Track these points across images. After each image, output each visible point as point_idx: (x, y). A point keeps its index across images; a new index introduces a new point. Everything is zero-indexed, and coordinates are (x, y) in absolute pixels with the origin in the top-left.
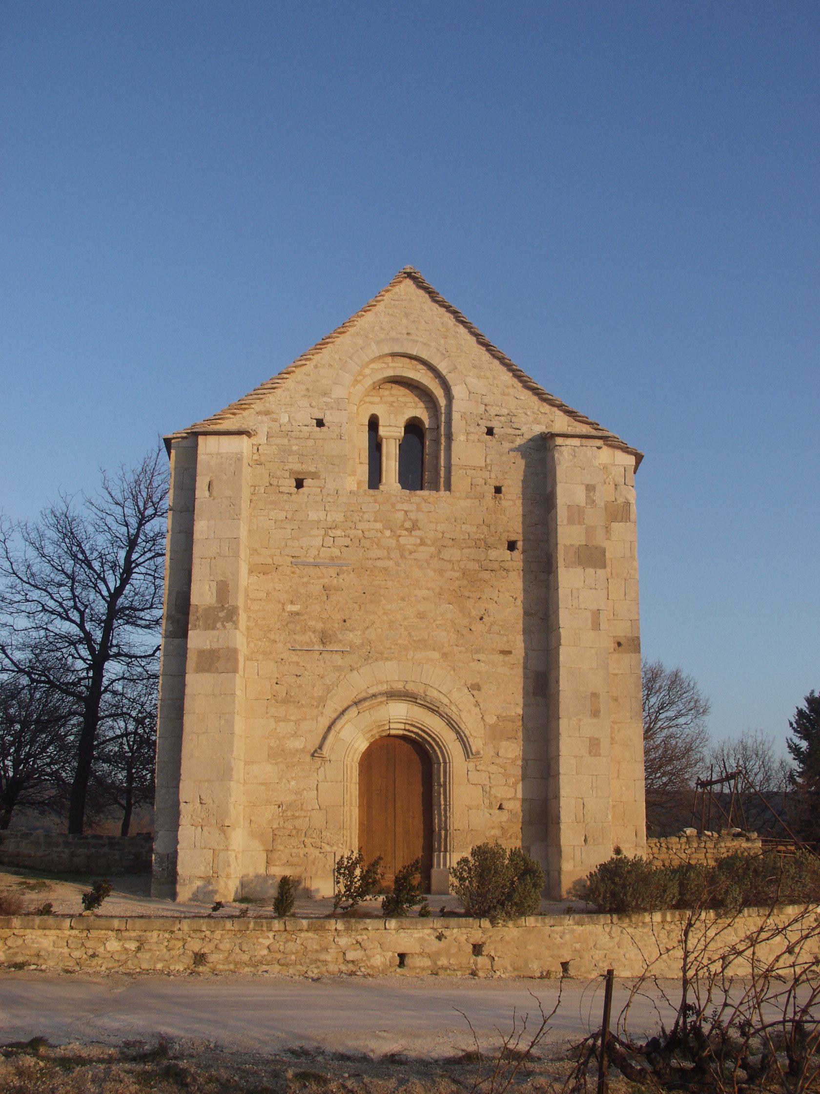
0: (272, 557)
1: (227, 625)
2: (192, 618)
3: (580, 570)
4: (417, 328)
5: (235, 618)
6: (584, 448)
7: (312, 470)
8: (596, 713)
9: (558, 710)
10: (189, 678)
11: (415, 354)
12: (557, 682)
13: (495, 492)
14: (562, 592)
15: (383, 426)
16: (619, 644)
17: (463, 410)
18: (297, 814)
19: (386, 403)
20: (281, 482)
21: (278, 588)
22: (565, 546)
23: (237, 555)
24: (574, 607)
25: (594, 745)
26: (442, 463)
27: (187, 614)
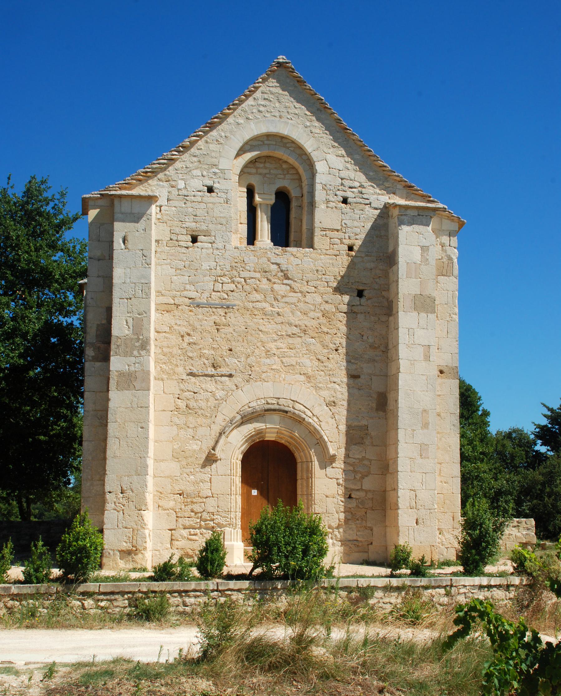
0: (174, 298)
1: (142, 352)
2: (113, 346)
3: (415, 314)
5: (148, 347)
6: (421, 217)
8: (425, 426)
9: (397, 423)
10: (111, 394)
11: (286, 134)
12: (397, 401)
13: (349, 250)
14: (402, 332)
16: (441, 372)
17: (324, 183)
18: (195, 500)
19: (260, 174)
20: (180, 237)
21: (179, 324)
22: (404, 295)
23: (148, 296)
24: (410, 343)
25: (423, 449)
26: (304, 227)
27: (109, 343)
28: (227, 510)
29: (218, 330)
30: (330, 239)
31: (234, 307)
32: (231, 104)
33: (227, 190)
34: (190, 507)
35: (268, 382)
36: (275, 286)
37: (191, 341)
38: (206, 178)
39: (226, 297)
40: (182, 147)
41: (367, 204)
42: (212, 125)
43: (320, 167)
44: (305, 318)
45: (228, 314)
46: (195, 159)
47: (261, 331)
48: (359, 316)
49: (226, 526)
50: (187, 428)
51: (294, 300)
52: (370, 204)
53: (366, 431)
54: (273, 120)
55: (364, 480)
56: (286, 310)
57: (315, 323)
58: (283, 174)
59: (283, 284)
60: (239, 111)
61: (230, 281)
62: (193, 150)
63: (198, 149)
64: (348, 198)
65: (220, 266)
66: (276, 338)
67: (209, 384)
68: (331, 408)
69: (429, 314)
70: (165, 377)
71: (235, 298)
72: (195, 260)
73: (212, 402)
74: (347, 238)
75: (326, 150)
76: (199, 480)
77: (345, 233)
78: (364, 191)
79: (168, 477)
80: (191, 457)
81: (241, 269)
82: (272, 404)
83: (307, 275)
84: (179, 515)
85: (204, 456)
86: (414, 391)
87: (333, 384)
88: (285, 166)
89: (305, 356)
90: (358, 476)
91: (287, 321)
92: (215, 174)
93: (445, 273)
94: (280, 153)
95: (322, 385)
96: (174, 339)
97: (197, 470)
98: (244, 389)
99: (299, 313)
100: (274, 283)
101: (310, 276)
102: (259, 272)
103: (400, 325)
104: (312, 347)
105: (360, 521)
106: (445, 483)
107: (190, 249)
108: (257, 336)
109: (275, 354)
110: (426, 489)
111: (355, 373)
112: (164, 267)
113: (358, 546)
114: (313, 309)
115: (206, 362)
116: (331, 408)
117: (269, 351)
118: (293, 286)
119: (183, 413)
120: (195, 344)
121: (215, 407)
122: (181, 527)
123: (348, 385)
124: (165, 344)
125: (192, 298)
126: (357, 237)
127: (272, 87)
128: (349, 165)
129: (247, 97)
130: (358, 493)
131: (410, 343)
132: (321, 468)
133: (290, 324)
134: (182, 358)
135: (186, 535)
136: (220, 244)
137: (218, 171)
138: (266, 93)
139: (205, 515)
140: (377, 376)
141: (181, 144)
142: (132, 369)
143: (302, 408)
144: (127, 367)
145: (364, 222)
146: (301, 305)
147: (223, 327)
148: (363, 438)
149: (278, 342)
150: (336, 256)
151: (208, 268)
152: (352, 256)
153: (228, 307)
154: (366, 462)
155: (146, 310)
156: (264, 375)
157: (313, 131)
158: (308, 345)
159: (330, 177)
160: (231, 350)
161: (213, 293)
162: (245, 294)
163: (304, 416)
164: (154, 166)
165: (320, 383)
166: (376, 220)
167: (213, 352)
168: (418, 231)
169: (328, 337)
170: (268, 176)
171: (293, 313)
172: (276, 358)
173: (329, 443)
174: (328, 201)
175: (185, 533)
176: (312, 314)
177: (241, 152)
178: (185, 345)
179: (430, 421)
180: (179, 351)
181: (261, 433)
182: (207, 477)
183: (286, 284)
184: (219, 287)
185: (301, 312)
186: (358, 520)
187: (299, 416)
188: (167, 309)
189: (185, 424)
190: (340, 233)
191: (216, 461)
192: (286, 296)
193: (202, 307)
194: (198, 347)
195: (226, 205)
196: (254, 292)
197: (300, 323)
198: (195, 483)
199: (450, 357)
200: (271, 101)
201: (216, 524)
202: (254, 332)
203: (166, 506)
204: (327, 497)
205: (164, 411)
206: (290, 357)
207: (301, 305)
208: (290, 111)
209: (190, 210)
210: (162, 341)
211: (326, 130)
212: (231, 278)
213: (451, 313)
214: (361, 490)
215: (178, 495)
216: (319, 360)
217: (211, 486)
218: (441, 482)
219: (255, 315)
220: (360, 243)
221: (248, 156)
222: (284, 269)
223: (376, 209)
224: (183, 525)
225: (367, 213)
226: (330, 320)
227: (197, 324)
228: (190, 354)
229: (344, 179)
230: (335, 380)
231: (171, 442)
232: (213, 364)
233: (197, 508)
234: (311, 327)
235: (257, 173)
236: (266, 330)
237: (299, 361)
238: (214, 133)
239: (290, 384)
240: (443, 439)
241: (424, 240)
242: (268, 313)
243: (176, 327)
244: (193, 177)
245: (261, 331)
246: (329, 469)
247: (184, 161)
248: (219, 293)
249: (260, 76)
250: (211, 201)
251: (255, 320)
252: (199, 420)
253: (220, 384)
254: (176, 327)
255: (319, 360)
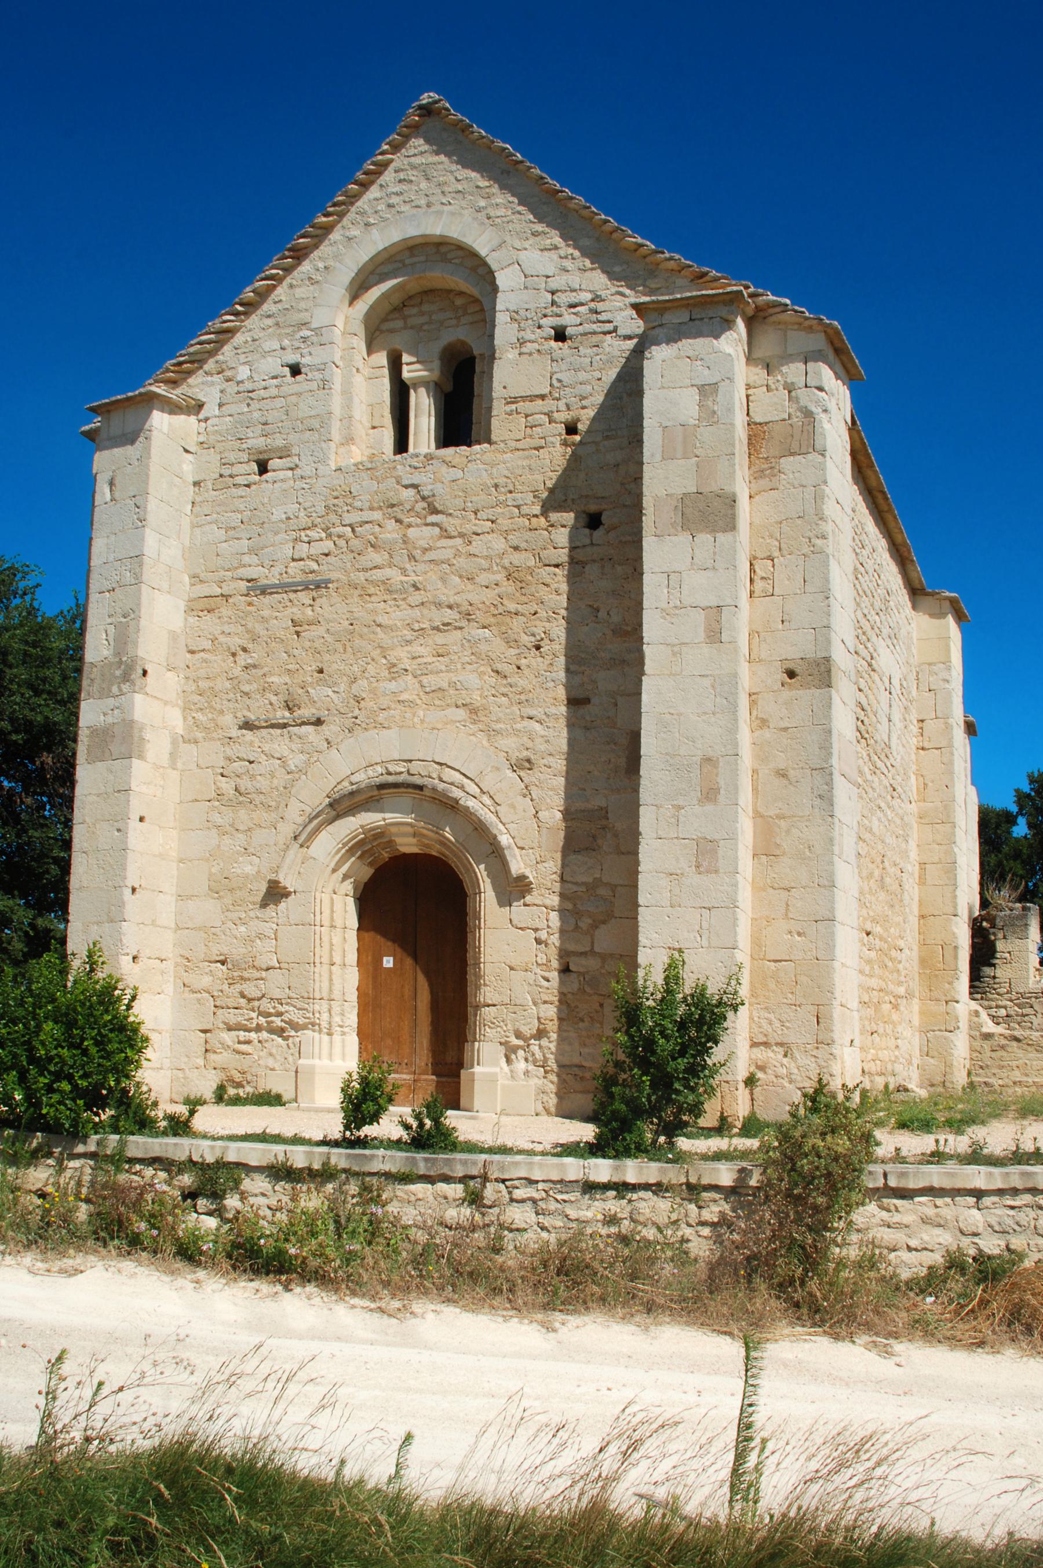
0: (220, 583)
3: (684, 537)
4: (443, 192)
6: (697, 322)
7: (281, 445)
15: (407, 364)
16: (791, 674)
17: (515, 308)
18: (246, 975)
19: (412, 328)
21: (227, 631)
24: (672, 604)
28: (306, 995)
29: (298, 633)
30: (527, 416)
31: (330, 585)
32: (330, 204)
33: (325, 364)
34: (238, 987)
35: (389, 728)
36: (412, 533)
37: (249, 661)
38: (289, 350)
39: (315, 566)
40: (241, 305)
41: (610, 333)
42: (300, 253)
43: (504, 279)
44: (470, 587)
45: (318, 600)
46: (269, 322)
47: (379, 625)
48: (588, 567)
49: (304, 1027)
50: (235, 832)
51: (448, 554)
52: (615, 330)
53: (604, 822)
54: (414, 215)
55: (597, 932)
56: (431, 578)
57: (490, 595)
58: (456, 318)
59: (427, 525)
60: (351, 215)
61: (324, 535)
62: (267, 307)
63: (275, 303)
64: (566, 327)
65: (305, 509)
66: (408, 638)
67: (278, 743)
68: (522, 774)
69: (718, 535)
70: (199, 735)
71: (331, 567)
72: (260, 507)
73: (281, 778)
74: (564, 408)
75: (518, 244)
76: (254, 934)
77: (558, 399)
78: (600, 306)
79: (200, 929)
80: (240, 889)
81: (345, 508)
82: (397, 774)
83: (474, 499)
84: (218, 1003)
85: (263, 887)
86: (680, 714)
87: (526, 723)
88: (459, 301)
89: (468, 667)
90: (585, 923)
91: (431, 599)
92: (304, 339)
93: (795, 447)
94: (441, 276)
95: (502, 726)
96: (219, 662)
97: (252, 914)
98: (342, 748)
99: (457, 579)
100: (409, 526)
101: (480, 499)
102: (380, 508)
103: (646, 568)
104: (483, 647)
105: (586, 1024)
106: (799, 934)
107: (254, 487)
108: (372, 636)
109: (406, 670)
110: (710, 947)
111: (580, 694)
112: (207, 528)
113: (582, 1078)
114: (486, 566)
115: (274, 699)
116: (522, 774)
117: (394, 665)
118: (445, 525)
119: (229, 804)
120: (255, 666)
121: (285, 788)
122: (222, 1026)
123: (568, 720)
124: (202, 673)
125: (252, 580)
126: (584, 403)
127: (415, 155)
128: (568, 264)
129: (365, 186)
130: (583, 961)
131: (672, 604)
132: (501, 904)
133: (439, 605)
134: (231, 696)
135: (230, 1043)
136: (309, 468)
137: (308, 333)
138: (402, 170)
139: (266, 1005)
140: (629, 695)
141: (237, 300)
142: (110, 720)
143: (457, 777)
144: (102, 718)
145: (600, 370)
146: (461, 562)
147: (307, 627)
148: (594, 837)
149: (415, 644)
150: (537, 449)
151: (284, 516)
152: (574, 444)
153: (318, 587)
154: (602, 891)
155: (135, 608)
156: (382, 716)
157: (492, 214)
158: (473, 643)
159: (525, 295)
160: (321, 671)
161: (292, 564)
162: (352, 556)
163: (456, 793)
164: (192, 350)
165: (498, 721)
166: (628, 359)
167: (287, 679)
168: (691, 354)
169: (517, 623)
170: (425, 327)
171: (443, 580)
172: (410, 677)
173: (517, 851)
174: (522, 342)
175: (229, 1038)
176: (483, 578)
177: (358, 288)
178: (237, 671)
179: (722, 783)
180: (228, 685)
181: (381, 835)
182: (268, 928)
183: (433, 524)
184: (303, 549)
185: (461, 577)
186: (582, 1020)
187: (444, 794)
188: (208, 606)
189: (232, 825)
190: (549, 401)
191: (286, 895)
192: (430, 549)
193: (271, 593)
194: (260, 672)
195: (321, 392)
196: (370, 549)
197: (458, 599)
198: (249, 940)
199: (812, 638)
200: (411, 181)
201: (285, 1022)
202: (365, 630)
203: (197, 986)
204: (512, 969)
205: (196, 800)
206: (437, 673)
207: (461, 562)
208: (446, 189)
209: (256, 415)
210: (198, 669)
211: (520, 204)
212: (326, 530)
213: (811, 535)
214: (592, 952)
215: (219, 964)
216: (497, 672)
217: (276, 946)
218: (790, 932)
219: (370, 595)
220: (592, 414)
221: (375, 293)
222: (426, 493)
223: (629, 337)
224: (225, 1023)
225: (607, 350)
226: (524, 585)
227: (259, 629)
228: (246, 688)
229: (557, 291)
230: (532, 712)
231: (207, 860)
232: (286, 702)
233: (251, 990)
234: (480, 606)
235: (405, 328)
236: (391, 622)
237: (454, 679)
238: (306, 267)
239: (433, 729)
240: (794, 830)
241: (706, 372)
242: (394, 588)
243: (222, 639)
244: (265, 354)
245: (379, 625)
246: (517, 908)
247: (250, 330)
248: (302, 563)
249: (384, 139)
250: (293, 392)
251: (370, 605)
252: (254, 815)
253: (298, 741)
254: (222, 639)
255: (497, 672)
